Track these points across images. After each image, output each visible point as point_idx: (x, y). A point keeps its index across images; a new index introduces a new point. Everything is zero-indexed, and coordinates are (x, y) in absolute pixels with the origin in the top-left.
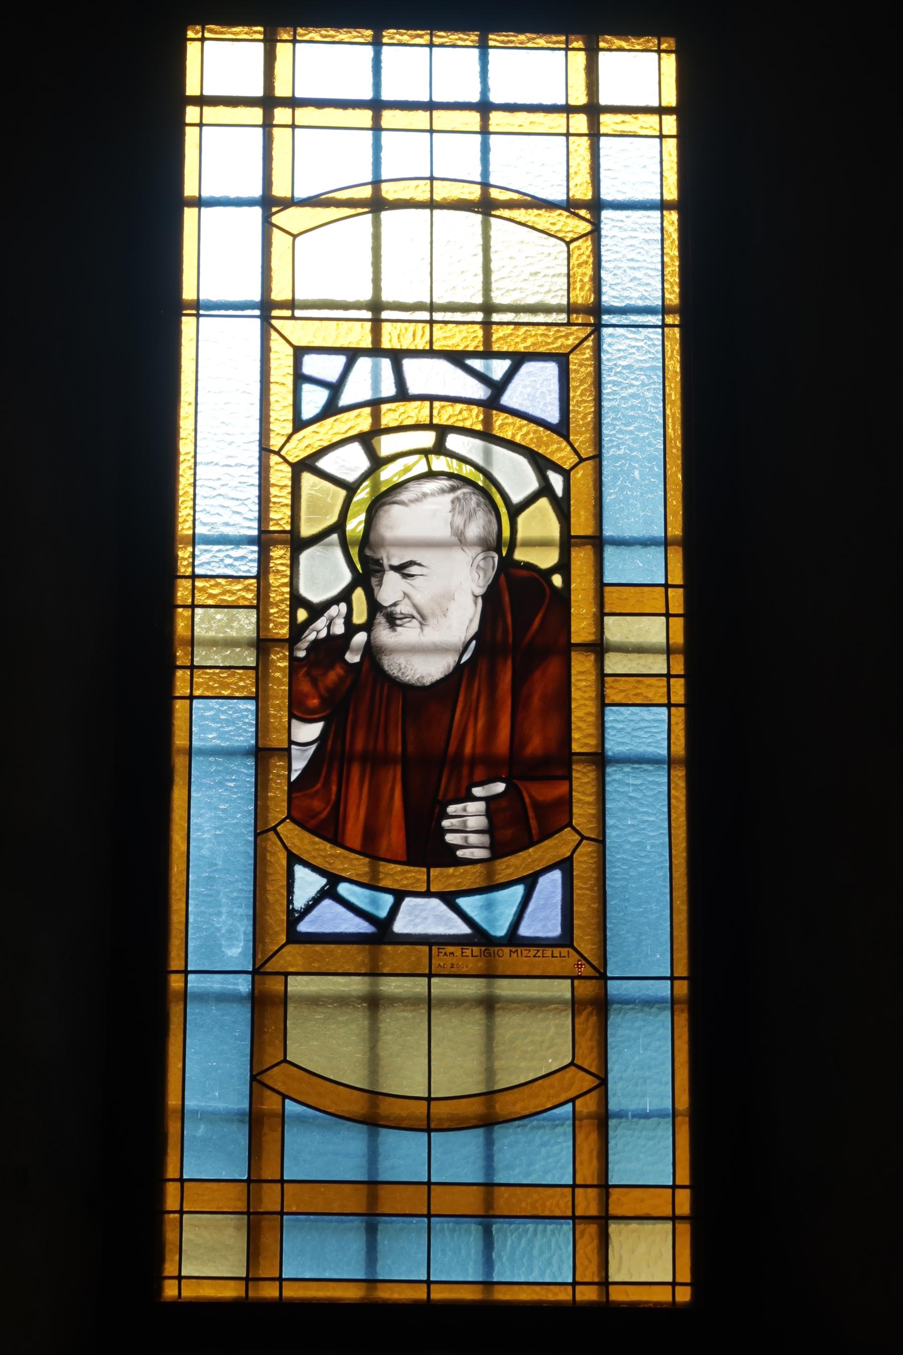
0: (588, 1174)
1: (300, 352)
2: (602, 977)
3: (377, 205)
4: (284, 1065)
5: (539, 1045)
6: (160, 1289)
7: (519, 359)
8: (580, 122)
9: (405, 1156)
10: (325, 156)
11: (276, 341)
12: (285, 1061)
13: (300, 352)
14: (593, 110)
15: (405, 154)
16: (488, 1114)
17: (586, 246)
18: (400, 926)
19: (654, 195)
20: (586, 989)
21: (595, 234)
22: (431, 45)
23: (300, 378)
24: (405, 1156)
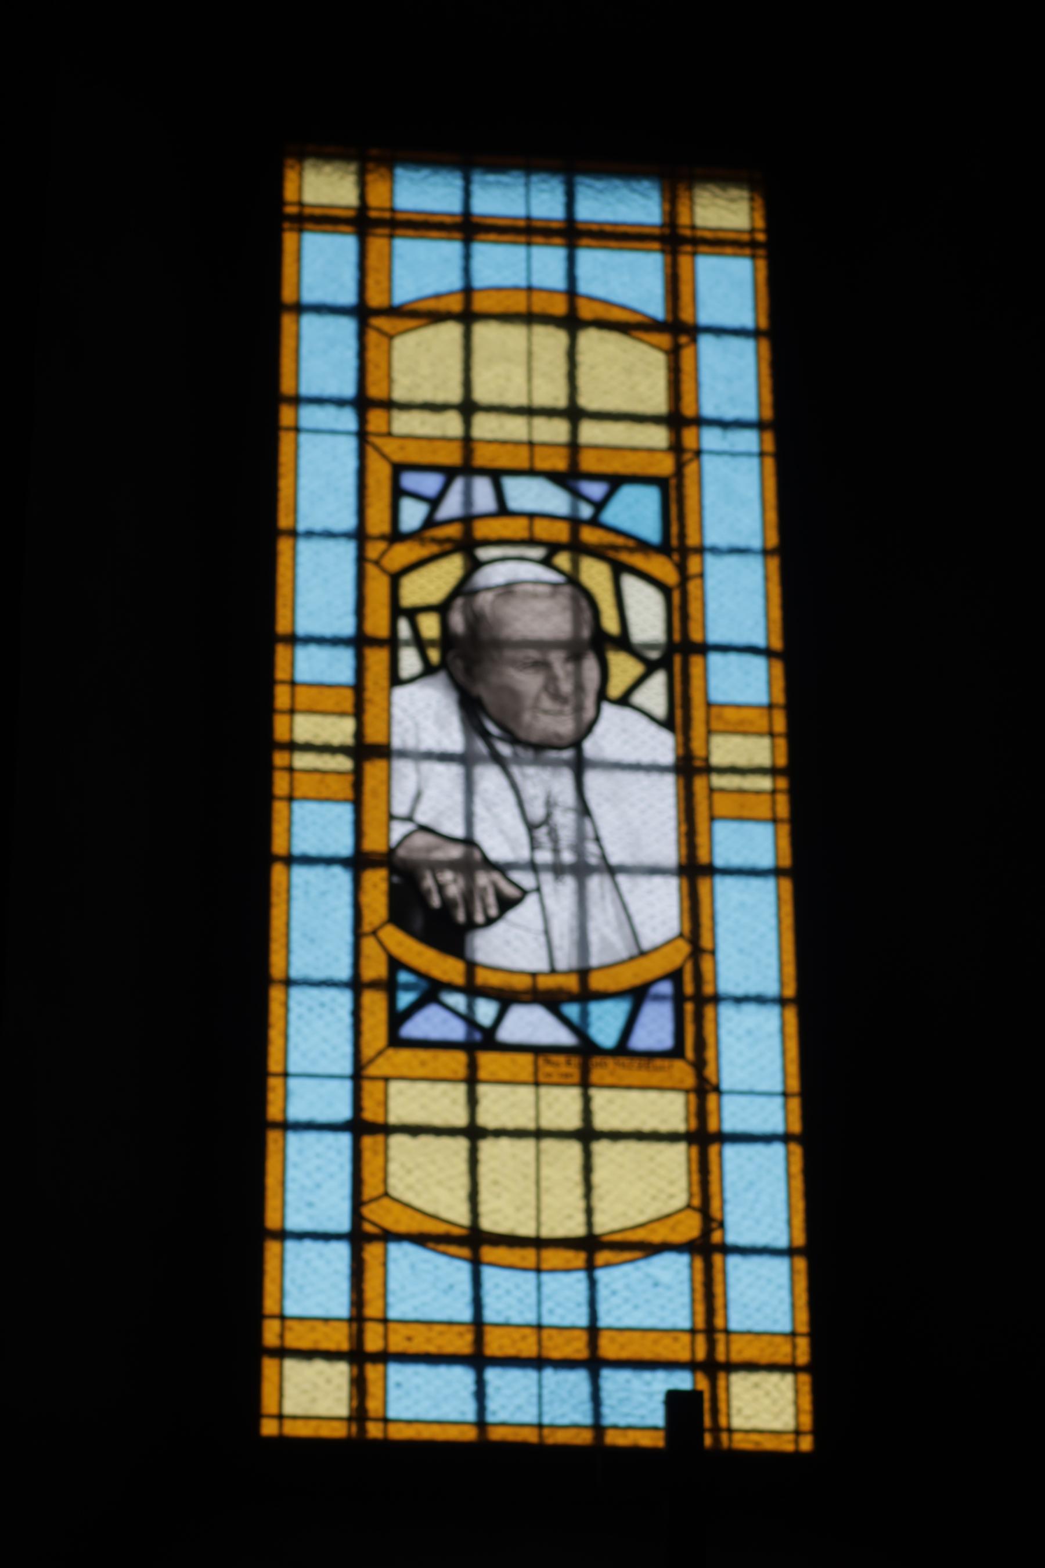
0: (701, 1324)
1: (398, 469)
2: (362, 436)
3: (468, 317)
4: (385, 1202)
5: (645, 1186)
6: (257, 1426)
7: (616, 482)
8: (373, 1343)
9: (512, 1295)
10: (651, 1297)
11: (372, 456)
12: (386, 1194)
13: (398, 469)
14: (357, 1357)
15: (498, 265)
16: (467, 312)
17: (370, 1190)
18: (507, 1033)
19: (291, 1245)
20: (376, 419)
21: (358, 1201)
22: (540, 1426)
23: (398, 493)
24: (512, 1295)
